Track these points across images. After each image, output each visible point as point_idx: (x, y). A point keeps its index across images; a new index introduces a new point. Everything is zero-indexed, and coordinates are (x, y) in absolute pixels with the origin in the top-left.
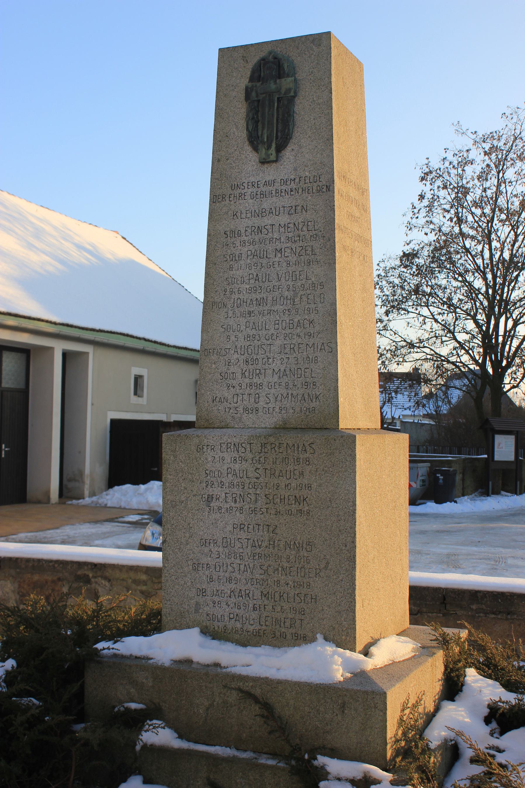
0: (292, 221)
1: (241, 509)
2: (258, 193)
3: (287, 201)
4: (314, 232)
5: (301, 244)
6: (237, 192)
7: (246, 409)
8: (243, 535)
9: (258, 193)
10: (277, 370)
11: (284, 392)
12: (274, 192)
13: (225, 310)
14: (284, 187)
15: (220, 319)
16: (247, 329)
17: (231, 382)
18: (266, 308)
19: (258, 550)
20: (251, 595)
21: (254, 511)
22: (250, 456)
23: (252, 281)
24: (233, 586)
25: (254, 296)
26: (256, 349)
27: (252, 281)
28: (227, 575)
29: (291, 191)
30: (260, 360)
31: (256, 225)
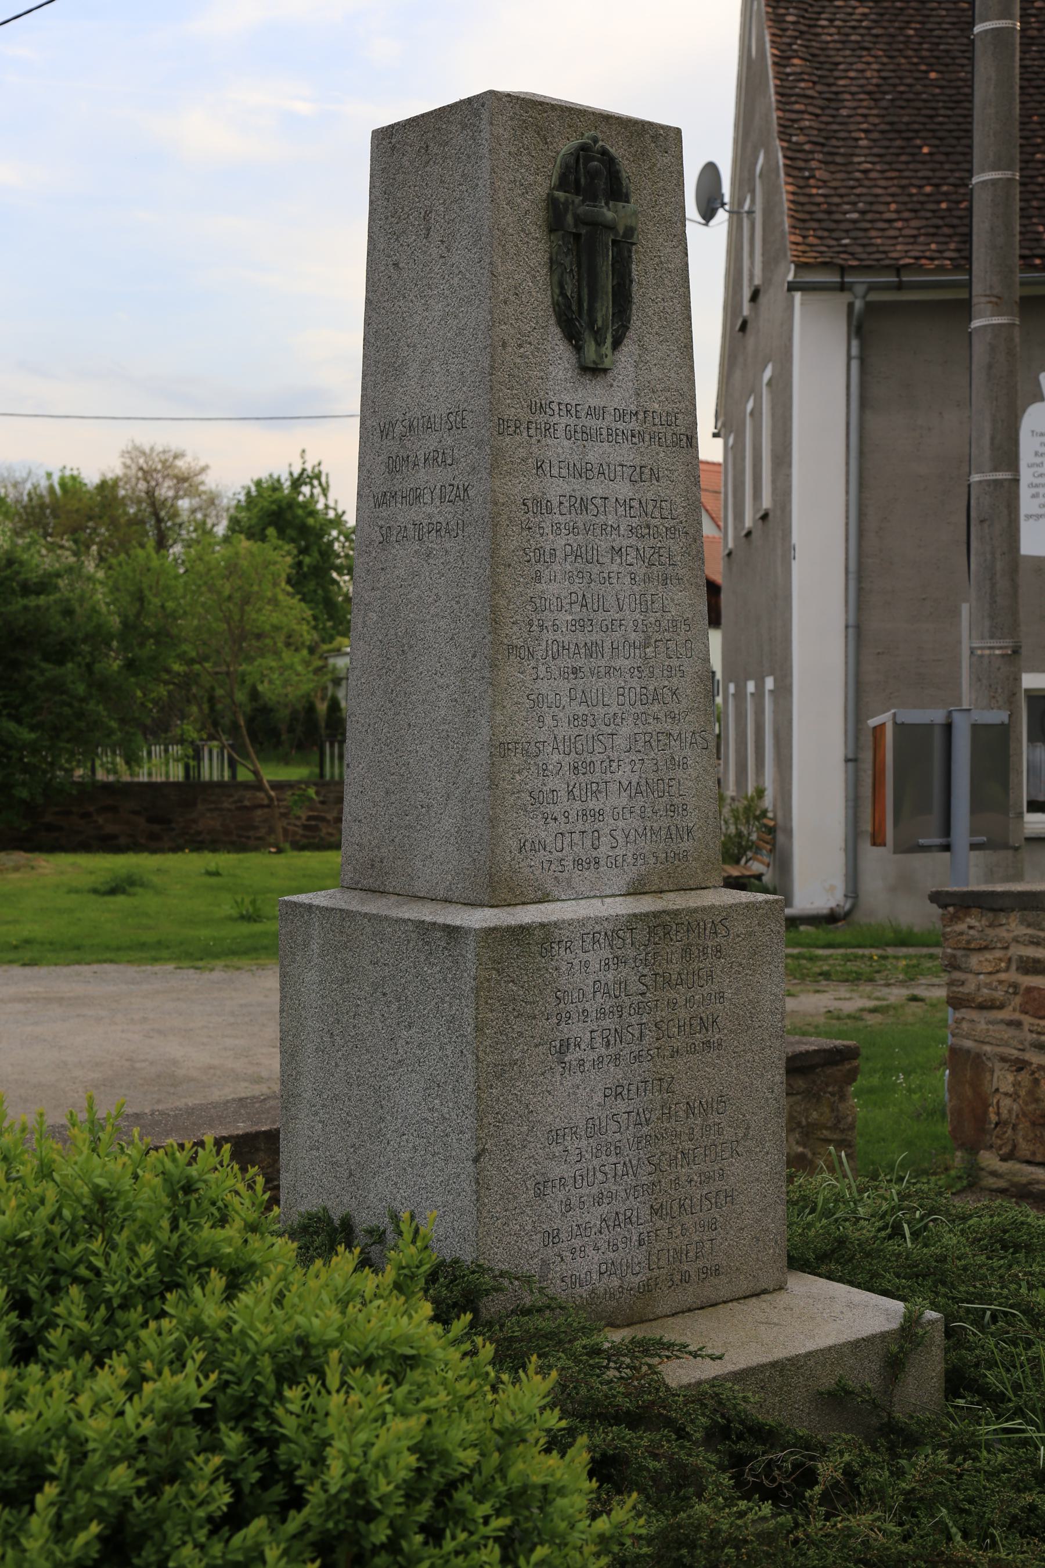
0: (637, 496)
1: (617, 1057)
2: (579, 429)
3: (624, 453)
4: (672, 523)
5: (652, 542)
6: (541, 418)
7: (578, 862)
8: (621, 1106)
9: (579, 429)
10: (625, 783)
11: (637, 823)
12: (604, 432)
13: (533, 663)
14: (621, 426)
15: (523, 681)
16: (573, 703)
17: (549, 809)
18: (603, 663)
19: (645, 1130)
20: (634, 1219)
21: (638, 1057)
22: (631, 953)
23: (576, 608)
24: (605, 1209)
25: (581, 638)
26: (590, 743)
27: (576, 608)
28: (595, 1190)
29: (633, 436)
30: (598, 764)
31: (578, 494)
